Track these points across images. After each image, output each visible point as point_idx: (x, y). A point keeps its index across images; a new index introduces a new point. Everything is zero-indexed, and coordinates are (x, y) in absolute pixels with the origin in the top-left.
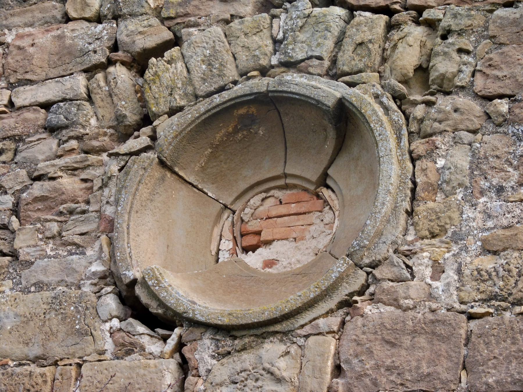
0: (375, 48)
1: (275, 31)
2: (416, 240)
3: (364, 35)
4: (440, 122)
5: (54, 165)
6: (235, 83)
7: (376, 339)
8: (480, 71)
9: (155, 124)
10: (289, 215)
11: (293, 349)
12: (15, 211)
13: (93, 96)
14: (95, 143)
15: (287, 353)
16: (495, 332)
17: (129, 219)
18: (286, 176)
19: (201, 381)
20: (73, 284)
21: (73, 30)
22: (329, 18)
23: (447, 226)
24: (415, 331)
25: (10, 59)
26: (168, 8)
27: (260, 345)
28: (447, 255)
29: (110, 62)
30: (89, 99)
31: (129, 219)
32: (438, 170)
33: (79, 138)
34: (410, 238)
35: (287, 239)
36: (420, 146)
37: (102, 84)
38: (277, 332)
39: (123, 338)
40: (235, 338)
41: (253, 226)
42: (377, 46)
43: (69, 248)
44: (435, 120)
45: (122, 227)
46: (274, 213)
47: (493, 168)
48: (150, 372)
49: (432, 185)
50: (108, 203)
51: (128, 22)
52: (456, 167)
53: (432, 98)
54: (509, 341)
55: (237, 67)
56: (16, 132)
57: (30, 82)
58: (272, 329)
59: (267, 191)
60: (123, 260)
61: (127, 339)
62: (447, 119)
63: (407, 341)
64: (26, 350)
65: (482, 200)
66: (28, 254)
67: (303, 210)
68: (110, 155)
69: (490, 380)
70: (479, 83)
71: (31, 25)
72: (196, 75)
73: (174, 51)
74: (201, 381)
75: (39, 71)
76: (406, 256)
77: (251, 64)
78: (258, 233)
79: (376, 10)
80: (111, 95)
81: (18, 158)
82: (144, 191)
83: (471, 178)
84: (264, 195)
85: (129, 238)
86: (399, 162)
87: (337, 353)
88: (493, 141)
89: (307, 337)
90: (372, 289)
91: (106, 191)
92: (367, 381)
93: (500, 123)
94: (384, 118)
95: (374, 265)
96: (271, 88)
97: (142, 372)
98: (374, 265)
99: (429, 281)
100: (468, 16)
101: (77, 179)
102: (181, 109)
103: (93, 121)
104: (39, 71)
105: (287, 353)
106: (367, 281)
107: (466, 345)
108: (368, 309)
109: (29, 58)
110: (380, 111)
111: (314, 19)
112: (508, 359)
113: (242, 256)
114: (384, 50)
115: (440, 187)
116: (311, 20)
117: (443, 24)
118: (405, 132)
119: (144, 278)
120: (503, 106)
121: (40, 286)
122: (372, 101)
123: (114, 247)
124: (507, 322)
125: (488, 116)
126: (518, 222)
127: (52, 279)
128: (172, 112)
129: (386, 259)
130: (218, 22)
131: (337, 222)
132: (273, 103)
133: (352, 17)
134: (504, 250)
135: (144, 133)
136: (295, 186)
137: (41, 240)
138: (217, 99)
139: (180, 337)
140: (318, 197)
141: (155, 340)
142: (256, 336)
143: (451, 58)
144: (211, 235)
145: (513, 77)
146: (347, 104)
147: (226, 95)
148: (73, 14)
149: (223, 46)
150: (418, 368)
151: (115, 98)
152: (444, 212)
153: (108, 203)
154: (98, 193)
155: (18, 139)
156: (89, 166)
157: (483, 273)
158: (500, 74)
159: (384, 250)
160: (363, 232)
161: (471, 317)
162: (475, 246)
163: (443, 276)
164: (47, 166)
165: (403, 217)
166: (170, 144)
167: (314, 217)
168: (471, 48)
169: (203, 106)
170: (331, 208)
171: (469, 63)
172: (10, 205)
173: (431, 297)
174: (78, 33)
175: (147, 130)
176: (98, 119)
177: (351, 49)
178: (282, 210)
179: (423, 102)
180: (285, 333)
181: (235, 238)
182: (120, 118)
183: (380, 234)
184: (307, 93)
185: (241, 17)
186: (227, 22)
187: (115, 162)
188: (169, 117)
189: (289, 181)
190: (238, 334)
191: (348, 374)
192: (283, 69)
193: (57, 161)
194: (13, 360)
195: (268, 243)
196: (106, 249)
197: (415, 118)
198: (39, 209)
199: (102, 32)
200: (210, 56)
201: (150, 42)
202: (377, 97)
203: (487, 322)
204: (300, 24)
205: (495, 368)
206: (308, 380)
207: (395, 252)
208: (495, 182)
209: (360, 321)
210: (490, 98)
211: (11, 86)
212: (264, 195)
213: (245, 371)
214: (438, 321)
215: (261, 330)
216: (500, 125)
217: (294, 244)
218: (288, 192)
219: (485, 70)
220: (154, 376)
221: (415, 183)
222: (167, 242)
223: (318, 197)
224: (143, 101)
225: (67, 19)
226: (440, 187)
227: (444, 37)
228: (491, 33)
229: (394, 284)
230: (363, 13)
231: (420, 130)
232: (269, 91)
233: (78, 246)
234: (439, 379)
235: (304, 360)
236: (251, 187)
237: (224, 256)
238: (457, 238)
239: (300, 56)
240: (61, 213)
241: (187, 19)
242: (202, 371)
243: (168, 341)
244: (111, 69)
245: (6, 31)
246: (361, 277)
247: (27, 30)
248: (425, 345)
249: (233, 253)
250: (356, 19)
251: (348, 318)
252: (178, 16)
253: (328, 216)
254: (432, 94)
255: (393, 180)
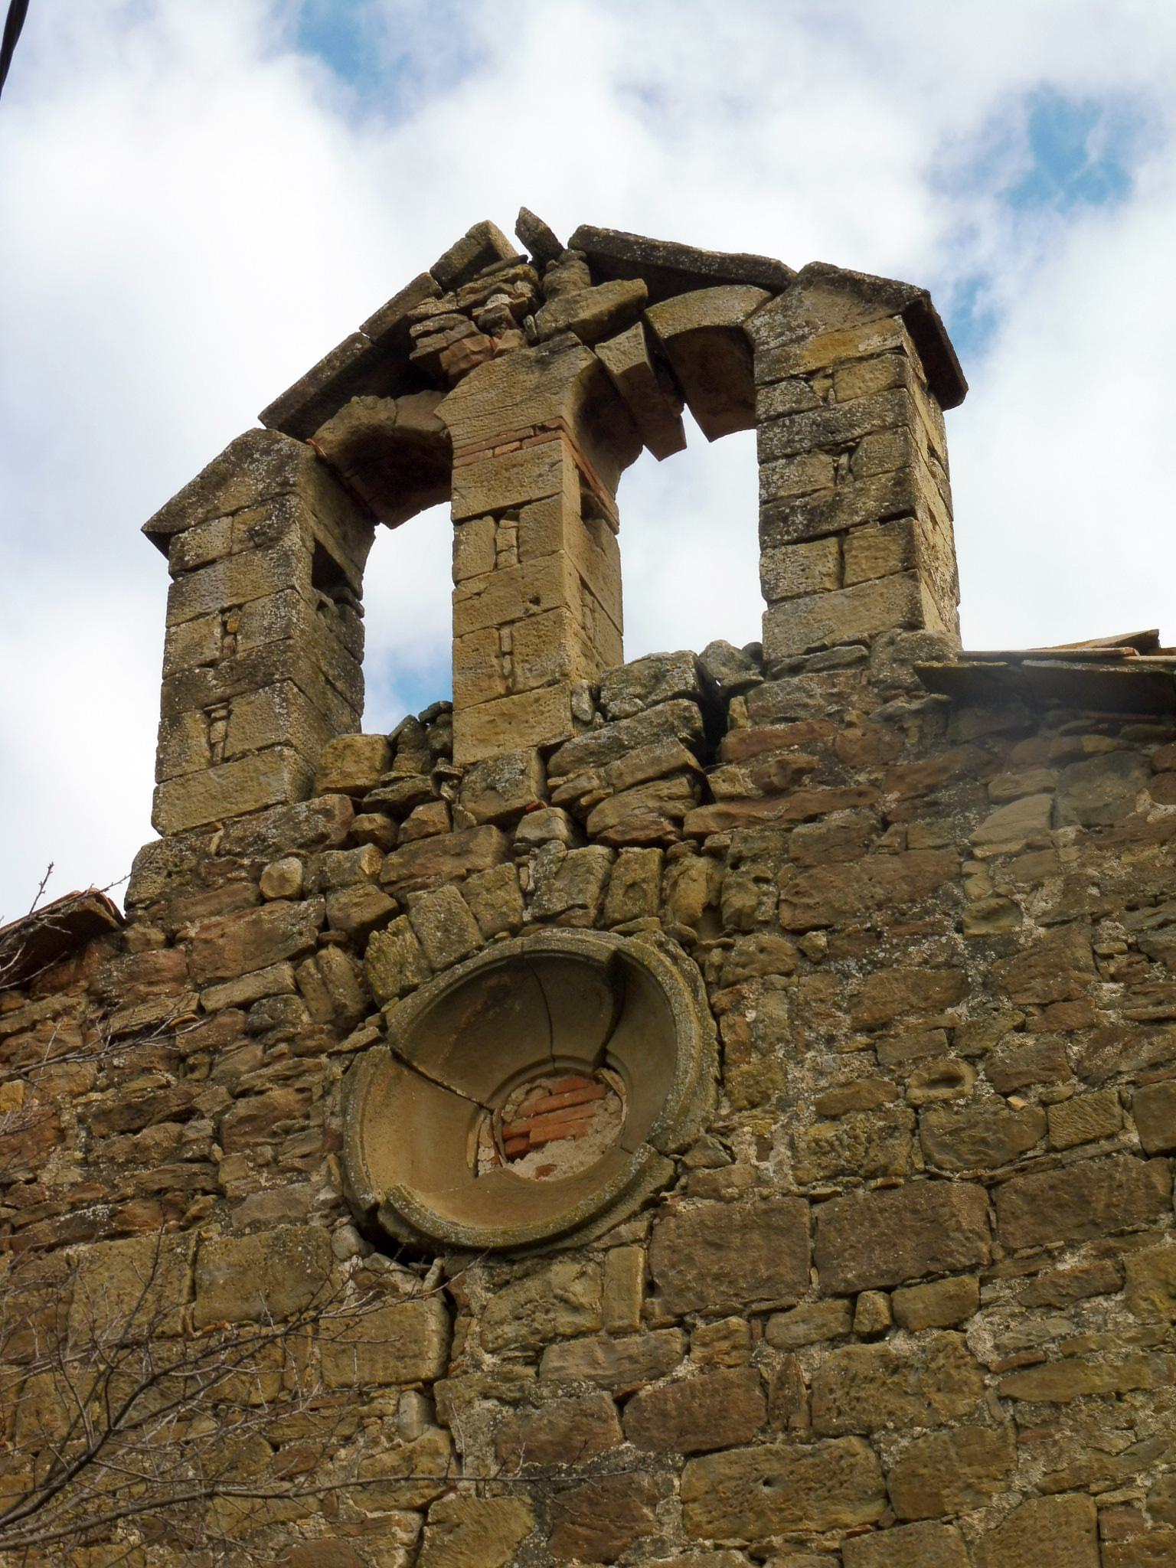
0: (651, 888)
1: (523, 882)
2: (732, 1113)
3: (636, 874)
4: (744, 966)
5: (260, 1076)
6: (480, 948)
7: (696, 1242)
8: (785, 901)
9: (383, 1009)
10: (563, 1108)
11: (590, 1268)
12: (217, 1137)
13: (302, 987)
14: (311, 1043)
15: (583, 1274)
16: (848, 1215)
17: (362, 1130)
18: (554, 1058)
19: (475, 1321)
20: (297, 1219)
21: (271, 913)
22: (589, 858)
23: (770, 1092)
24: (745, 1226)
25: (195, 956)
26: (387, 872)
27: (547, 1268)
28: (774, 1127)
29: (321, 944)
30: (298, 991)
31: (362, 1130)
32: (748, 1024)
33: (290, 1040)
34: (724, 1112)
35: (563, 1138)
36: (721, 998)
37: (313, 970)
38: (567, 1249)
39: (369, 1278)
40: (512, 1262)
41: (518, 1126)
42: (652, 885)
43: (289, 1175)
44: (737, 965)
45: (353, 1140)
46: (543, 1107)
47: (818, 1014)
48: (407, 1317)
49: (743, 1044)
50: (332, 1113)
51: (339, 895)
52: (770, 1018)
53: (730, 940)
54: (867, 1224)
55: (481, 929)
56: (210, 1041)
57: (223, 980)
58: (560, 1245)
59: (532, 1080)
60: (360, 1181)
61: (374, 1279)
62: (752, 962)
63: (736, 1240)
64: (246, 1307)
65: (809, 1055)
66: (237, 1188)
67: (580, 1099)
68: (330, 1056)
69: (849, 1276)
70: (786, 914)
71: (219, 913)
72: (431, 944)
73: (401, 920)
74: (475, 1321)
75: (232, 965)
76: (722, 1134)
77: (499, 922)
78: (525, 1135)
79: (645, 844)
80: (325, 984)
81: (215, 1073)
82: (377, 1094)
83: (792, 1030)
84: (527, 1086)
85: (363, 1153)
86: (699, 1019)
87: (648, 1267)
88: (810, 983)
89: (606, 1250)
90: (683, 1181)
91: (329, 1100)
92: (691, 1296)
93: (816, 960)
94: (674, 969)
95: (683, 1150)
96: (527, 949)
97: (398, 1317)
98: (683, 1150)
99: (754, 1161)
100: (763, 838)
101: (291, 1090)
102: (414, 988)
103: (305, 1018)
104: (232, 965)
105: (583, 1274)
106: (675, 1171)
107: (812, 1236)
108: (682, 1206)
109: (219, 951)
110: (668, 961)
111: (571, 862)
112: (869, 1246)
113: (509, 1166)
114: (662, 890)
115: (754, 1046)
116: (568, 864)
117: (732, 850)
118: (701, 983)
119: (388, 1201)
120: (821, 939)
121: (256, 1226)
122: (656, 950)
123: (345, 1167)
124: (861, 1201)
125: (803, 954)
126: (858, 1077)
127: (271, 1215)
128: (405, 992)
129: (697, 1141)
130: (452, 879)
131: (625, 1109)
132: (532, 968)
133: (617, 855)
134: (845, 1113)
135: (371, 1024)
136: (567, 1071)
137: (252, 1169)
138: (460, 970)
139: (442, 1269)
140: (598, 1081)
141: (410, 1277)
142: (541, 1257)
143: (746, 890)
144: (466, 1144)
145: (828, 903)
146: (625, 957)
147: (470, 964)
148: (270, 894)
149: (460, 906)
150: (754, 1271)
151: (330, 986)
152: (763, 1074)
153: (332, 1113)
154: (318, 1104)
155: (212, 1050)
156: (305, 1072)
157: (823, 1144)
158: (811, 901)
159: (694, 1129)
160: (664, 1110)
161: (815, 1200)
162: (808, 1112)
163: (773, 1153)
164: (252, 1078)
165: (712, 1088)
166: (405, 1031)
167: (595, 1106)
168: (770, 876)
169: (442, 981)
170: (615, 1094)
171: (771, 893)
172: (209, 1131)
173: (760, 1181)
174: (277, 916)
175: (373, 1019)
176: (311, 1015)
177: (621, 892)
178: (554, 1102)
179: (718, 946)
180: (578, 1249)
181: (496, 1144)
182: (338, 1009)
183: (685, 1110)
184: (574, 949)
185: (479, 871)
186: (462, 879)
187: (337, 1063)
188: (401, 998)
189: (559, 1065)
190: (515, 1257)
191: (665, 1291)
192: (538, 926)
193: (264, 1071)
194: (231, 1322)
195: (539, 1146)
196: (335, 1170)
197: (712, 965)
198: (246, 1133)
199: (307, 909)
200: (446, 920)
201: (368, 914)
202: (661, 945)
203: (836, 1204)
204: (554, 869)
205: (853, 1259)
206: (615, 1304)
207: (707, 1132)
208: (822, 1031)
209: (672, 1223)
210: (800, 932)
211: (198, 988)
212: (527, 1086)
213: (531, 1301)
214: (773, 1210)
215: (546, 1248)
216: (818, 963)
217: (573, 1143)
218: (559, 1079)
219: (790, 899)
220: (414, 1321)
221: (722, 1044)
222: (402, 1158)
223: (598, 1081)
224: (366, 986)
225: (263, 900)
226: (754, 1046)
227: (735, 867)
228: (792, 855)
229: (712, 1171)
230: (630, 849)
231: (719, 979)
232: (524, 953)
233: (300, 1171)
234: (783, 1282)
235: (606, 1281)
236: (512, 1078)
237: (485, 1168)
238: (784, 1104)
239: (559, 907)
240: (274, 1134)
241: (412, 882)
242: (475, 1307)
243: (428, 1275)
244: (323, 952)
245: (188, 924)
246: (668, 1168)
247: (214, 919)
248: (761, 1242)
249: (496, 1162)
250: (624, 857)
251: (656, 1221)
252: (401, 879)
253: (613, 1104)
254: (729, 935)
255: (694, 1042)
